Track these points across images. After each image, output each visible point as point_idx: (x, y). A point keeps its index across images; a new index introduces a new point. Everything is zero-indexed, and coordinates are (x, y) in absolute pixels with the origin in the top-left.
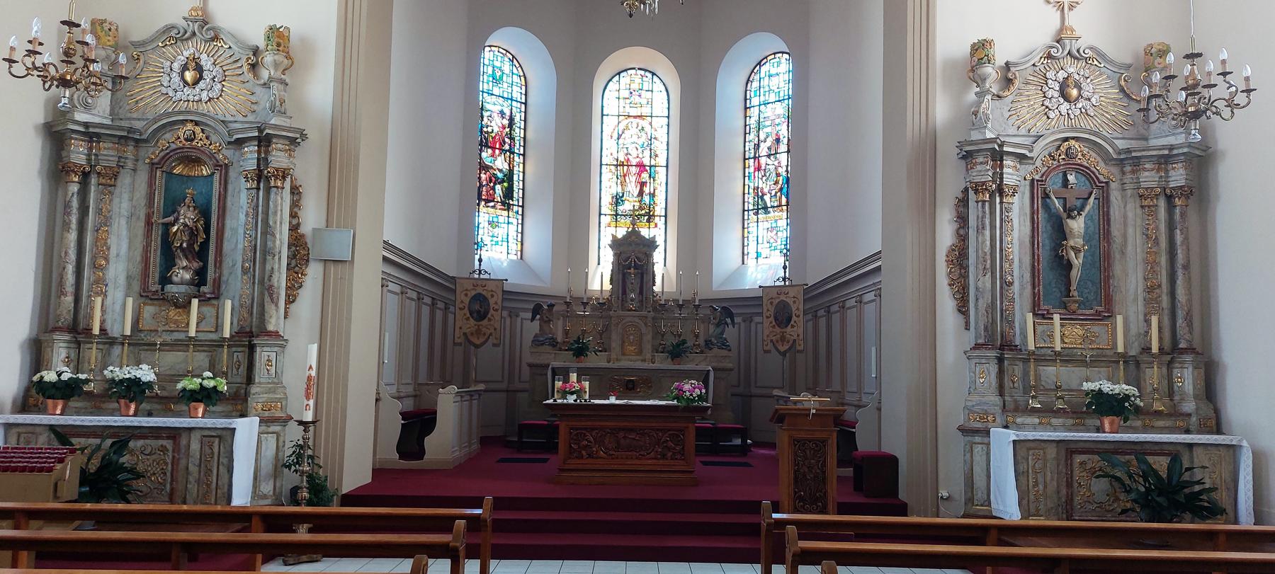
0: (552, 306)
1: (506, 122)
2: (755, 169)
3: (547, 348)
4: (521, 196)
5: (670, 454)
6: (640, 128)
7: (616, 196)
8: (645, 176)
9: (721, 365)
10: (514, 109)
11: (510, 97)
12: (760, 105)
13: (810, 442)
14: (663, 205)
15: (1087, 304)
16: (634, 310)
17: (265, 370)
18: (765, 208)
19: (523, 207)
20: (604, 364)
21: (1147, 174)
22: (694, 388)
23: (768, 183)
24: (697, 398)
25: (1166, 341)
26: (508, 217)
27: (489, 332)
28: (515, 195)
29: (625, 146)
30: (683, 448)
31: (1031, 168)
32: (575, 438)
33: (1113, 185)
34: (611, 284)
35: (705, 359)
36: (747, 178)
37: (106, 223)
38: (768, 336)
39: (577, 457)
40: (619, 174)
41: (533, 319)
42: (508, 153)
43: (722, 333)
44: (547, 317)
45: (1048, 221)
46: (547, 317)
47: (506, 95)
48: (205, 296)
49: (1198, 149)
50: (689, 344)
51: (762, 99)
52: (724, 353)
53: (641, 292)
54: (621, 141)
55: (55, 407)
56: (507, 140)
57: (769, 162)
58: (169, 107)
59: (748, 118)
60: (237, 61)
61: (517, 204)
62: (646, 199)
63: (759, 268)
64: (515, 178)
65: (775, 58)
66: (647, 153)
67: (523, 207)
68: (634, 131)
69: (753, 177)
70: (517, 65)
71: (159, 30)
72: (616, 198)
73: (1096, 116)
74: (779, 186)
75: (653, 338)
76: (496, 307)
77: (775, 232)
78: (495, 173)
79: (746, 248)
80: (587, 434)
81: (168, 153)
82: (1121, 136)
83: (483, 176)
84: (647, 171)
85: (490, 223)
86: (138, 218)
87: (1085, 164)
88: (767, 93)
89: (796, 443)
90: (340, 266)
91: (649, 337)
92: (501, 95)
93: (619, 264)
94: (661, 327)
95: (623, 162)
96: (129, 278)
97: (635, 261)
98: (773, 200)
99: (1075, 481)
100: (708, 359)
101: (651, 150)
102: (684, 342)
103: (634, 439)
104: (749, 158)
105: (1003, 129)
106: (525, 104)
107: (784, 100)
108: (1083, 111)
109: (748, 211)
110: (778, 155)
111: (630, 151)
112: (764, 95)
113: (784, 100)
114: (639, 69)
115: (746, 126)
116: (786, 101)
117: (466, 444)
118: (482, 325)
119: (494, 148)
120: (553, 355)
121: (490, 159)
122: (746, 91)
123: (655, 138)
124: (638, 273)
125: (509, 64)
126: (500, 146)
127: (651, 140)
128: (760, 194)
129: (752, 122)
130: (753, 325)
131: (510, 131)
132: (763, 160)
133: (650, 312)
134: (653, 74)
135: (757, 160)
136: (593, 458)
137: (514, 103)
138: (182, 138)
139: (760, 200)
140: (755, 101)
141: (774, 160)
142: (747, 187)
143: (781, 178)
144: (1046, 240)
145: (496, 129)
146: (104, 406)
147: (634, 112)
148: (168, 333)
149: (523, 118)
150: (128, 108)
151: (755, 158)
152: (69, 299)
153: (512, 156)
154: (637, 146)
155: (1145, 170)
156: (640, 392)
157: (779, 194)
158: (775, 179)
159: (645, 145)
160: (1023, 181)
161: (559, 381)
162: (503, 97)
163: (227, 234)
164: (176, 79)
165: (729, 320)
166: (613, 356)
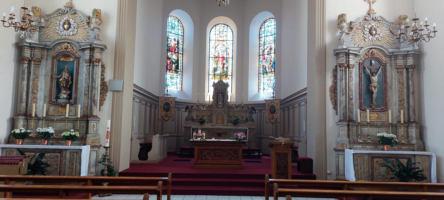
0: (192, 107)
1: (176, 43)
2: (263, 59)
3: (191, 121)
4: (181, 68)
5: (233, 158)
6: (223, 45)
7: (215, 68)
8: (225, 61)
9: (251, 127)
10: (179, 38)
11: (178, 34)
12: (264, 37)
13: (282, 154)
14: (231, 72)
15: (379, 106)
16: (221, 108)
17: (92, 129)
18: (267, 73)
19: (182, 72)
20: (210, 127)
21: (399, 60)
22: (242, 135)
23: (267, 64)
24: (243, 139)
25: (406, 119)
26: (177, 76)
27: (170, 116)
28: (179, 68)
29: (218, 51)
30: (238, 156)
31: (359, 58)
32: (200, 152)
33: (388, 65)
34: (213, 99)
35: (245, 125)
36: (260, 62)
37: (37, 78)
38: (267, 117)
39: (201, 159)
40: (215, 61)
41: (186, 111)
42: (177, 53)
43: (251, 116)
44: (190, 111)
45: (365, 77)
46: (190, 111)
47: (176, 33)
48: (71, 103)
49: (417, 52)
50: (240, 120)
51: (265, 34)
52: (252, 123)
53: (223, 102)
54: (216, 49)
55: (19, 142)
56: (176, 49)
57: (268, 56)
58: (59, 37)
59: (260, 41)
60: (82, 21)
61: (180, 71)
62: (225, 69)
63: (264, 93)
64: (179, 62)
65: (270, 20)
66: (225, 53)
67: (182, 72)
68: (221, 45)
69: (262, 62)
70: (180, 23)
71: (56, 10)
72: (215, 69)
73: (382, 40)
74: (271, 65)
75: (227, 118)
76: (173, 107)
77: (270, 81)
78: (172, 60)
79: (260, 86)
80: (205, 151)
81: (59, 53)
82: (390, 47)
83: (168, 61)
84: (225, 60)
85: (171, 78)
86: (48, 76)
87: (378, 57)
88: (267, 33)
89: (277, 154)
90: (118, 93)
91: (226, 117)
92: (175, 33)
93: (216, 92)
94: (230, 114)
95: (217, 57)
96: (45, 97)
97: (221, 91)
98: (269, 70)
99: (374, 168)
100: (247, 125)
101: (227, 52)
102: (238, 119)
103: (221, 153)
104: (261, 55)
105: (349, 45)
106: (183, 36)
107: (273, 35)
108: (377, 39)
109: (261, 73)
110: (271, 54)
111: (219, 53)
112: (266, 33)
113: (273, 35)
114: (223, 24)
115: (260, 44)
116: (274, 35)
117: (162, 155)
118: (168, 113)
119: (172, 52)
120: (193, 124)
121: (170, 55)
122: (260, 32)
123: (228, 48)
124: (222, 95)
125: (177, 22)
126: (174, 51)
127: (227, 49)
128: (265, 68)
129: (262, 42)
130: (262, 113)
131: (178, 46)
132: (266, 56)
133: (226, 109)
134: (228, 26)
135: (264, 56)
136: (206, 160)
137: (179, 36)
138: (63, 48)
139: (265, 70)
140: (263, 35)
141: (269, 56)
142: (260, 65)
143: (272, 62)
144: (364, 84)
145: (173, 45)
146: (36, 141)
147: (221, 39)
148: (59, 116)
149: (182, 41)
150: (44, 37)
151: (263, 55)
152: (24, 104)
153: (178, 54)
154: (222, 51)
155: (399, 59)
156: (223, 136)
157: (271, 67)
158: (270, 62)
159: (225, 50)
160: (356, 63)
161: (195, 133)
162: (175, 34)
163: (79, 81)
164: (61, 27)
165: (254, 112)
166: (214, 124)
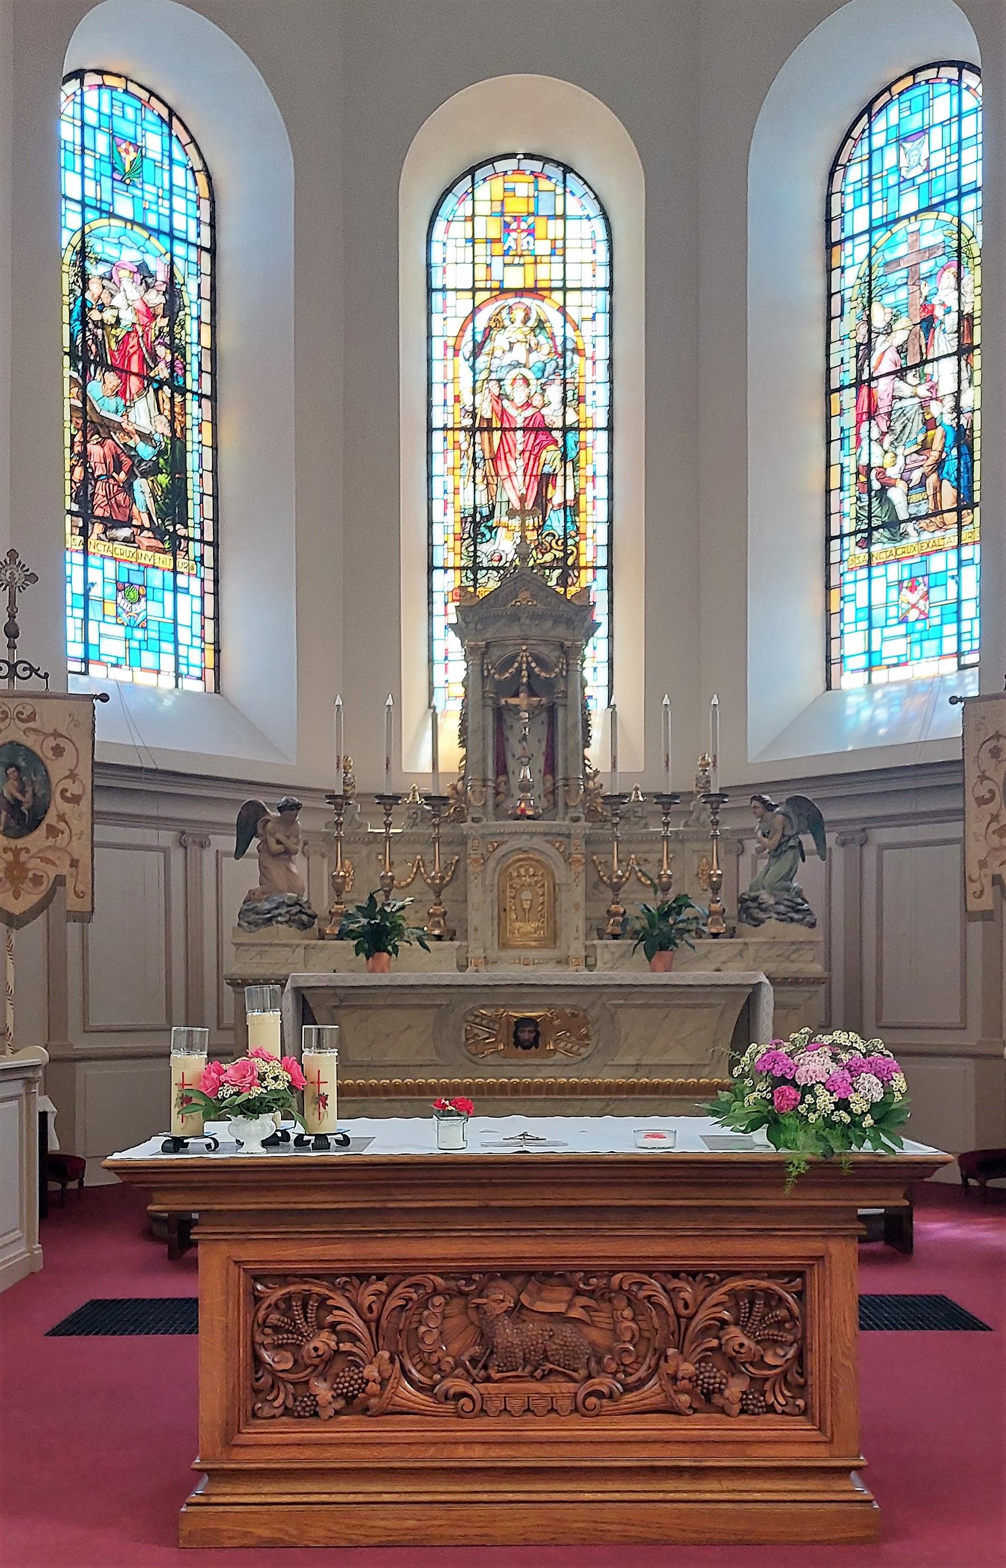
0: (290, 809)
1: (156, 299)
2: (859, 416)
3: (283, 932)
4: (209, 513)
6: (532, 323)
7: (474, 516)
8: (551, 455)
9: (791, 969)
10: (179, 263)
11: (167, 229)
14: (602, 538)
16: (529, 817)
19: (215, 544)
20: (449, 975)
22: (854, 1070)
23: (900, 451)
24: (868, 1121)
26: (175, 571)
27: (52, 872)
28: (193, 511)
29: (493, 376)
30: (800, 1357)
32: (274, 1318)
34: (463, 744)
35: (740, 954)
36: (835, 446)
38: (983, 864)
39: (287, 1412)
40: (479, 454)
41: (240, 852)
42: (166, 388)
43: (789, 876)
44: (279, 842)
46: (279, 842)
47: (152, 221)
50: (699, 908)
51: (878, 210)
52: (798, 932)
53: (551, 767)
54: (482, 362)
56: (161, 351)
59: (836, 274)
61: (198, 537)
62: (556, 521)
63: (878, 695)
64: (192, 461)
65: (915, 85)
66: (554, 393)
67: (215, 544)
68: (516, 331)
69: (853, 439)
70: (185, 139)
72: (474, 521)
74: (934, 455)
75: (587, 898)
76: (74, 789)
78: (132, 443)
79: (835, 644)
80: (340, 1301)
83: (95, 450)
84: (556, 442)
85: (121, 587)
91: (579, 892)
92: (139, 220)
94: (608, 865)
95: (489, 421)
97: (529, 669)
98: (915, 498)
100: (751, 950)
101: (564, 383)
102: (682, 903)
103: (561, 1318)
104: (842, 388)
106: (212, 251)
107: (944, 202)
109: (841, 537)
110: (928, 368)
111: (508, 389)
113: (944, 202)
114: (529, 156)
115: (830, 296)
116: (953, 207)
117: (18, 1233)
118: (27, 851)
119: (124, 373)
120: (301, 951)
121: (114, 402)
122: (829, 196)
123: (576, 351)
124: (540, 706)
125: (159, 130)
126: (141, 368)
127: (563, 356)
128: (876, 485)
129: (849, 281)
130: (870, 854)
131: (171, 324)
132: (883, 388)
133: (576, 820)
134: (567, 169)
135: (865, 391)
136: (365, 1411)
137: (179, 249)
139: (875, 504)
140: (859, 221)
141: (916, 381)
142: (835, 471)
143: (939, 432)
145: (128, 317)
147: (514, 278)
149: (206, 293)
153: (178, 398)
154: (525, 372)
156: (555, 1051)
157: (933, 479)
159: (550, 369)
161: (190, 1048)
162: (144, 226)
165: (808, 841)
166: (476, 952)
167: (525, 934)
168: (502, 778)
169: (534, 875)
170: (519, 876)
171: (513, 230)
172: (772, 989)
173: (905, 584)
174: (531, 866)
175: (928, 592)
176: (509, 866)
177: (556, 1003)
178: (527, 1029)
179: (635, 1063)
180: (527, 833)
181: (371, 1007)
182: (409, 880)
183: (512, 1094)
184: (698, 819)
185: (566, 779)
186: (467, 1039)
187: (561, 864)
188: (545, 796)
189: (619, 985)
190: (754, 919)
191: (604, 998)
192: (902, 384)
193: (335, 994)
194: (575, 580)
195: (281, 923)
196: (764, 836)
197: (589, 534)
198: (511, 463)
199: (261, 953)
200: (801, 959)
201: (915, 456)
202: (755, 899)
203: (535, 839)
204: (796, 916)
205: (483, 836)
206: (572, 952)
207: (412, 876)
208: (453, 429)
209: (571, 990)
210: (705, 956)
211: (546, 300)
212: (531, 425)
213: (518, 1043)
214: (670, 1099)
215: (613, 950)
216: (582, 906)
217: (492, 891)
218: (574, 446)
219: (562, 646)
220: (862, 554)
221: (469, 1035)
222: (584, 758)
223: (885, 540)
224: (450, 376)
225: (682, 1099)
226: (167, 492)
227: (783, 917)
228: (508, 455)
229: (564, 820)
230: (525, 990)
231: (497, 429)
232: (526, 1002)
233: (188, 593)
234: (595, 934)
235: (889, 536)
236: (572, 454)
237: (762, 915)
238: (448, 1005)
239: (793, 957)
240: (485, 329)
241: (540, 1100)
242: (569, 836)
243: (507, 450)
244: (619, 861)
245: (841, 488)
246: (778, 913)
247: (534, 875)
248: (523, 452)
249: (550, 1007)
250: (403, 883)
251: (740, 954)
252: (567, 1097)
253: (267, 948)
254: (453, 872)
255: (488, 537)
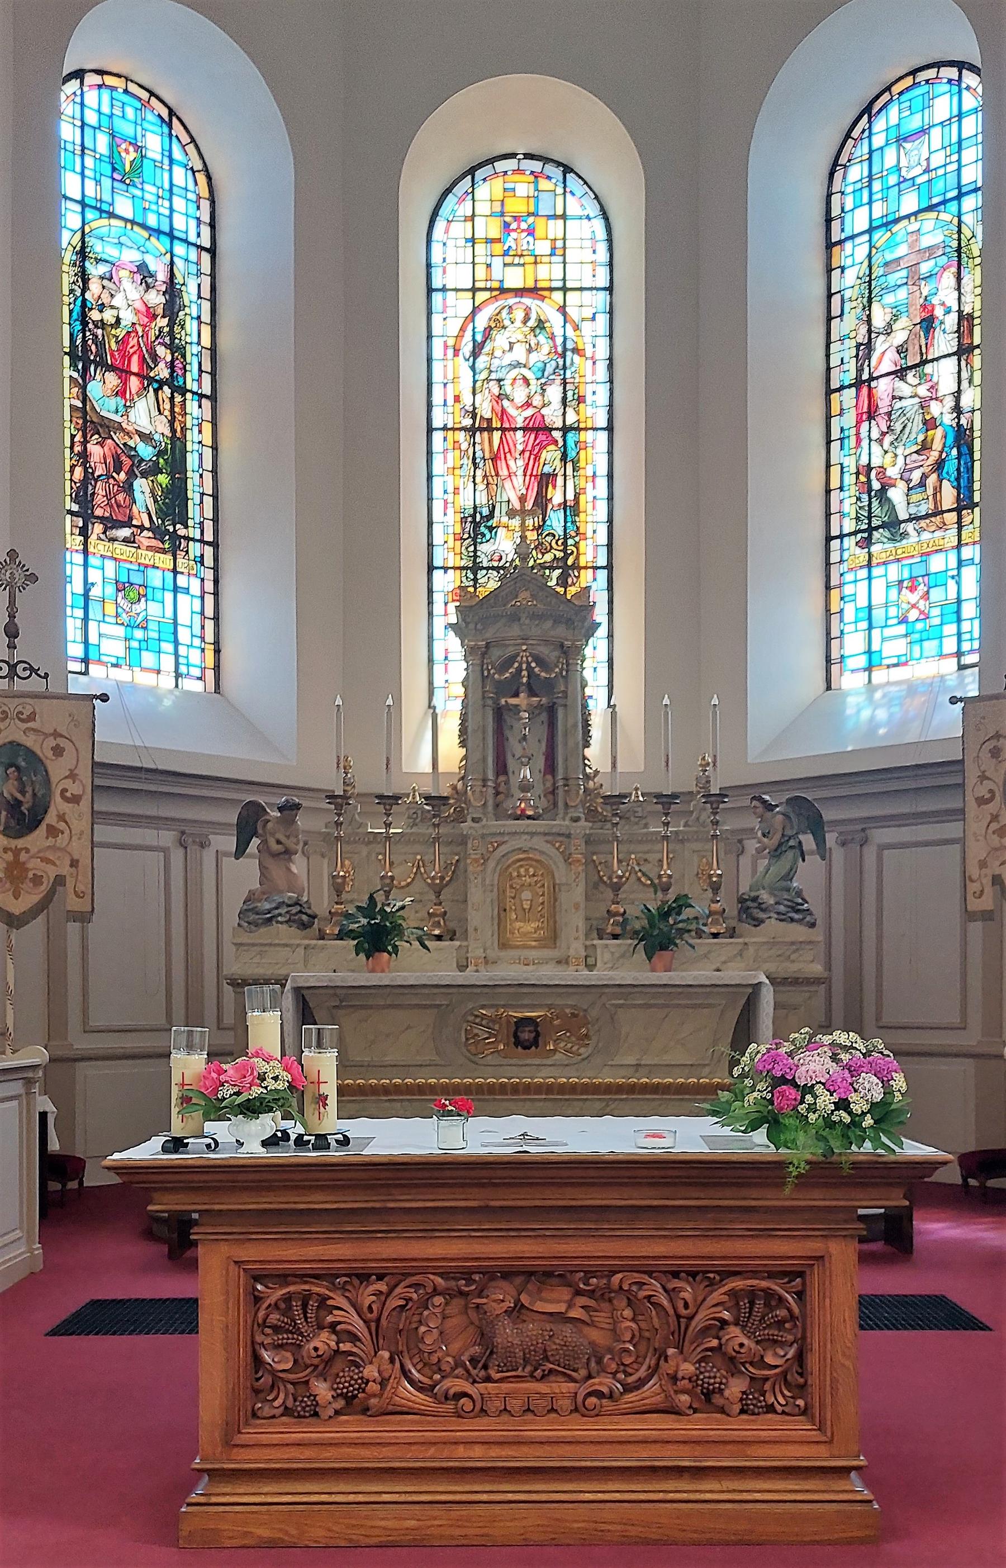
0: (290, 809)
1: (156, 299)
2: (859, 416)
3: (283, 932)
4: (209, 513)
6: (532, 323)
7: (474, 516)
8: (551, 455)
9: (791, 969)
10: (179, 263)
11: (167, 229)
14: (602, 538)
16: (529, 817)
19: (215, 544)
20: (449, 975)
22: (854, 1070)
23: (900, 451)
24: (868, 1121)
26: (175, 571)
27: (52, 872)
28: (193, 511)
29: (493, 376)
30: (800, 1357)
32: (274, 1318)
34: (463, 744)
35: (740, 954)
36: (835, 446)
38: (983, 864)
39: (287, 1412)
40: (479, 454)
41: (240, 852)
42: (166, 388)
43: (789, 876)
44: (279, 842)
46: (279, 842)
47: (152, 221)
50: (699, 908)
51: (878, 210)
52: (798, 932)
53: (551, 767)
54: (482, 362)
56: (161, 351)
59: (836, 274)
61: (198, 537)
62: (556, 521)
63: (878, 695)
64: (192, 461)
65: (915, 85)
66: (554, 393)
67: (215, 544)
68: (516, 331)
69: (853, 439)
70: (185, 139)
72: (474, 521)
74: (934, 455)
75: (587, 898)
76: (74, 789)
78: (132, 443)
79: (835, 644)
80: (340, 1301)
83: (95, 450)
84: (556, 442)
85: (121, 587)
91: (579, 892)
92: (139, 220)
94: (608, 865)
95: (489, 421)
97: (529, 669)
98: (915, 498)
100: (751, 950)
101: (564, 383)
102: (682, 903)
103: (561, 1318)
104: (842, 388)
106: (212, 251)
107: (944, 202)
109: (841, 537)
110: (928, 368)
111: (508, 389)
113: (944, 202)
114: (529, 156)
115: (830, 296)
116: (953, 207)
117: (18, 1233)
118: (27, 851)
119: (124, 373)
120: (301, 951)
121: (114, 402)
122: (829, 196)
123: (576, 351)
124: (540, 706)
125: (159, 130)
126: (141, 368)
127: (563, 356)
128: (876, 485)
129: (849, 281)
130: (870, 854)
131: (171, 324)
132: (883, 388)
133: (576, 820)
134: (567, 169)
135: (865, 391)
136: (365, 1411)
137: (179, 249)
139: (875, 504)
140: (859, 221)
141: (916, 381)
142: (835, 471)
143: (939, 432)
145: (128, 317)
147: (514, 278)
149: (206, 293)
153: (178, 398)
154: (525, 372)
156: (555, 1051)
157: (933, 479)
159: (550, 369)
161: (190, 1048)
162: (144, 226)
165: (808, 841)
166: (476, 952)
167: (525, 934)
168: (502, 778)
169: (534, 875)
170: (519, 876)
171: (513, 230)
172: (772, 989)
173: (905, 584)
174: (531, 866)
175: (928, 592)
176: (509, 866)
177: (556, 1003)
178: (527, 1029)
179: (635, 1063)
180: (527, 833)
181: (371, 1007)
182: (409, 880)
183: (512, 1094)
184: (698, 819)
185: (566, 779)
186: (467, 1039)
187: (561, 864)
188: (545, 796)
189: (619, 985)
190: (754, 919)
191: (604, 998)
192: (902, 384)
193: (335, 994)
194: (575, 580)
195: (281, 923)
196: (764, 836)
197: (589, 534)
198: (511, 463)
199: (261, 953)
200: (801, 959)
201: (915, 456)
202: (755, 899)
203: (535, 839)
204: (796, 916)
205: (483, 836)
206: (572, 952)
207: (412, 876)
208: (453, 429)
209: (571, 990)
210: (705, 956)
211: (546, 300)
212: (531, 425)
213: (518, 1043)
214: (670, 1099)
215: (613, 950)
216: (582, 906)
217: (492, 891)
218: (574, 446)
219: (562, 646)
220: (862, 554)
221: (469, 1035)
222: (584, 758)
223: (885, 540)
224: (450, 376)
225: (682, 1099)
226: (167, 492)
227: (783, 917)
228: (508, 455)
229: (564, 820)
230: (525, 990)
231: (497, 429)
232: (526, 1002)
233: (188, 593)
234: (595, 934)
235: (889, 536)
236: (572, 454)
237: (762, 915)
238: (448, 1005)
239: (793, 957)
240: (485, 329)
241: (540, 1100)
242: (569, 836)
243: (507, 450)
244: (619, 861)
245: (841, 488)
246: (778, 913)
247: (534, 875)
248: (523, 452)
249: (550, 1007)
250: (403, 883)
251: (740, 954)
252: (567, 1097)
253: (267, 948)
254: (453, 872)
255: (488, 537)
